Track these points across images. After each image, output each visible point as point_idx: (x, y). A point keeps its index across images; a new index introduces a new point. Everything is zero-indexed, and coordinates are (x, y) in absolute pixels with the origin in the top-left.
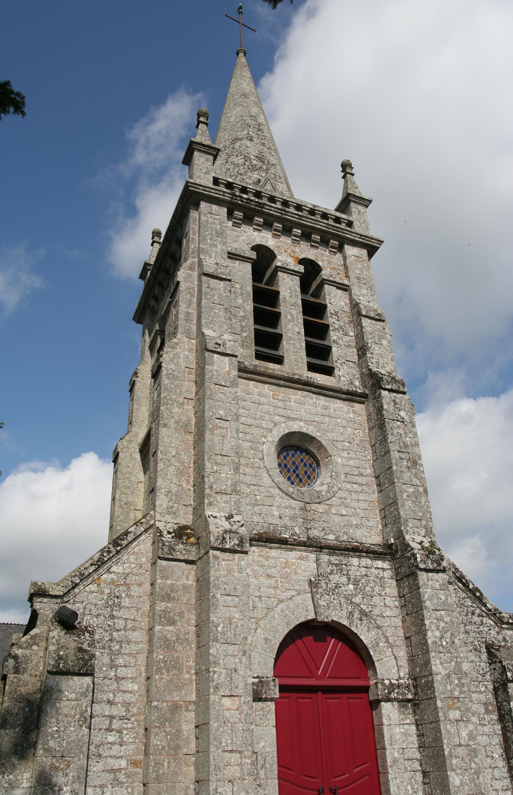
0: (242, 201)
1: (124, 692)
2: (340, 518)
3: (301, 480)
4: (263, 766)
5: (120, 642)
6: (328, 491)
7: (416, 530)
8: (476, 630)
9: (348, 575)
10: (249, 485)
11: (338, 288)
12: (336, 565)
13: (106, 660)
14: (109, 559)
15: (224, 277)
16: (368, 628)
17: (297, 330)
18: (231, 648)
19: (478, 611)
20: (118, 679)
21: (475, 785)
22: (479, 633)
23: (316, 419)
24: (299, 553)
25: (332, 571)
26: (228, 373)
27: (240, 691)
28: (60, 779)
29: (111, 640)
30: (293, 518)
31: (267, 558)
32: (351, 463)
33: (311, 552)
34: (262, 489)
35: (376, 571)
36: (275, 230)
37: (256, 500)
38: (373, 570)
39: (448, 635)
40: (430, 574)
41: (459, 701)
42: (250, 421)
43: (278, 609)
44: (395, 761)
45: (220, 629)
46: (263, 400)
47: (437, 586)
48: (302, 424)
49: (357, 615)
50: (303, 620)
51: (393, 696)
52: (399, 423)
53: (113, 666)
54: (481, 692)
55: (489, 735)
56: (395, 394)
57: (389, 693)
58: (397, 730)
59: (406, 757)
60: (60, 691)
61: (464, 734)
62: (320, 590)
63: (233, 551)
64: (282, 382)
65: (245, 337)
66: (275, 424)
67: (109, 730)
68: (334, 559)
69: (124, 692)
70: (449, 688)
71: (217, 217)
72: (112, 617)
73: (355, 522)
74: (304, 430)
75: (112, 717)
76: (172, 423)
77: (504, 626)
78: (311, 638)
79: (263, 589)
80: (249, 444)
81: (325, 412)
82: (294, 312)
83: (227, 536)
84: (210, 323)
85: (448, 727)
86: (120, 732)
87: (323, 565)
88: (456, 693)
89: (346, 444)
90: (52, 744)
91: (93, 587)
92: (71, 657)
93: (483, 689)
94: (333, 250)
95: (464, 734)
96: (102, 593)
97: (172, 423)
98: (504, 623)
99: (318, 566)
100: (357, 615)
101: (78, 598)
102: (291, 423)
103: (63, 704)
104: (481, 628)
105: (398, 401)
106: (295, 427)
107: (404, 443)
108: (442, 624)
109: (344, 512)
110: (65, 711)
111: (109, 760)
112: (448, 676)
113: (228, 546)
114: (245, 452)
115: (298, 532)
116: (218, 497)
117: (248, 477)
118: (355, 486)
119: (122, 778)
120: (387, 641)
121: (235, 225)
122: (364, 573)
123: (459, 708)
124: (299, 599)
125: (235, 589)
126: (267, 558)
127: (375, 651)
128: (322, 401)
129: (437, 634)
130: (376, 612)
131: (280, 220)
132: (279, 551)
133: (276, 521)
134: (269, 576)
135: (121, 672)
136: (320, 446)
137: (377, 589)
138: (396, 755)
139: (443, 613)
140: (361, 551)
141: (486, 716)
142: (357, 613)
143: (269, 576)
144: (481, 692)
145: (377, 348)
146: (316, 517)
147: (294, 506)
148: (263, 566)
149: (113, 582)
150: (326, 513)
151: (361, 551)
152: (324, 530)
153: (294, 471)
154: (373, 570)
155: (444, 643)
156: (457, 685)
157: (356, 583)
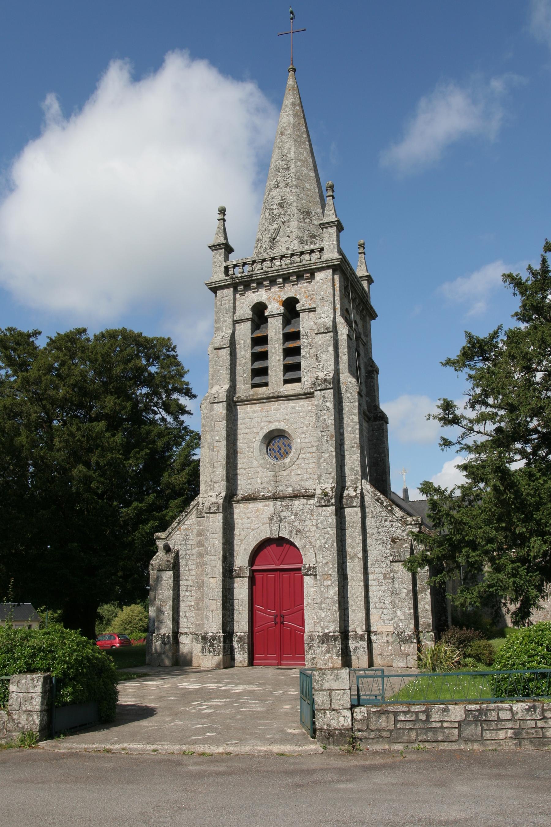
0: (239, 280)
1: (192, 575)
2: (297, 477)
3: (282, 456)
4: (241, 605)
5: (190, 555)
6: (290, 462)
7: (327, 480)
8: (386, 531)
9: (291, 510)
10: (245, 469)
11: (309, 312)
12: (285, 506)
13: (184, 563)
14: (183, 519)
15: (225, 346)
16: (301, 538)
17: (278, 358)
18: (213, 557)
19: (390, 519)
20: (189, 570)
21: (334, 617)
22: (388, 532)
23: (287, 417)
24: (264, 503)
25: (282, 510)
26: (221, 413)
27: (217, 575)
28: (164, 609)
29: (186, 554)
30: (268, 482)
31: (247, 509)
32: (307, 440)
33: (271, 501)
34: (252, 469)
35: (309, 506)
36: (266, 287)
37: (249, 476)
38: (308, 506)
39: (330, 541)
40: (324, 508)
41: (331, 576)
42: (247, 431)
43: (252, 534)
44: (309, 604)
45: (209, 549)
46: (255, 415)
47: (328, 514)
48: (277, 423)
49: (294, 532)
50: (264, 538)
51: (309, 573)
52: (325, 411)
53: (187, 565)
54: (383, 567)
55: (384, 591)
56: (324, 391)
57: (308, 571)
58: (312, 589)
59: (315, 602)
60: (162, 577)
61: (331, 593)
62: (273, 522)
63: (215, 513)
64: (265, 401)
65: (245, 377)
66: (262, 428)
67: (187, 591)
68: (284, 503)
69: (192, 575)
70: (326, 569)
71: (227, 298)
72: (186, 544)
73: (306, 478)
74: (279, 427)
75: (187, 586)
76: (206, 445)
77: (408, 526)
78: (275, 545)
79: (245, 525)
80: (246, 445)
81: (293, 411)
82: (277, 346)
83: (212, 506)
84: (218, 381)
85: (322, 589)
86: (191, 591)
87: (278, 507)
88: (330, 572)
89: (305, 428)
90: (160, 597)
91: (178, 532)
92: (164, 564)
93: (384, 566)
94: (308, 281)
95: (331, 593)
96: (182, 534)
97: (206, 445)
98: (408, 525)
99: (275, 508)
100: (294, 532)
101: (173, 538)
102: (270, 425)
103: (163, 582)
104: (391, 529)
105: (326, 395)
106: (273, 426)
107: (326, 425)
108: (327, 536)
109: (299, 473)
110: (164, 585)
111: (187, 602)
112: (327, 564)
113: (212, 511)
114: (244, 450)
115: (271, 490)
116: (215, 485)
117: (245, 464)
118: (307, 455)
119: (192, 609)
120: (311, 544)
121: (241, 295)
122: (301, 508)
123: (331, 580)
124: (263, 528)
125: (216, 530)
126: (247, 509)
127: (303, 550)
128: (291, 404)
129: (323, 541)
130: (306, 529)
131: (266, 279)
132: (254, 504)
133: (259, 486)
134: (248, 518)
135: (190, 567)
136: (289, 434)
137: (308, 516)
138: (310, 601)
139: (329, 529)
140: (299, 496)
141: (384, 581)
142: (295, 531)
143: (248, 518)
144: (383, 567)
145: (324, 356)
146: (282, 480)
147: (269, 475)
148: (245, 513)
149: (186, 529)
150: (288, 475)
151: (299, 496)
152: (286, 485)
153: (278, 451)
154: (308, 506)
155: (327, 546)
156: (331, 568)
157: (296, 514)
